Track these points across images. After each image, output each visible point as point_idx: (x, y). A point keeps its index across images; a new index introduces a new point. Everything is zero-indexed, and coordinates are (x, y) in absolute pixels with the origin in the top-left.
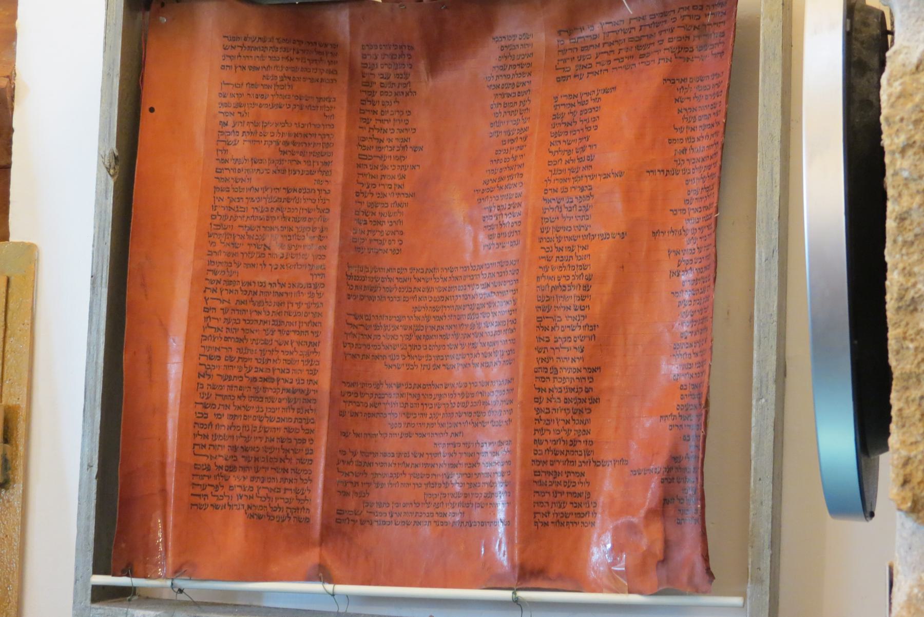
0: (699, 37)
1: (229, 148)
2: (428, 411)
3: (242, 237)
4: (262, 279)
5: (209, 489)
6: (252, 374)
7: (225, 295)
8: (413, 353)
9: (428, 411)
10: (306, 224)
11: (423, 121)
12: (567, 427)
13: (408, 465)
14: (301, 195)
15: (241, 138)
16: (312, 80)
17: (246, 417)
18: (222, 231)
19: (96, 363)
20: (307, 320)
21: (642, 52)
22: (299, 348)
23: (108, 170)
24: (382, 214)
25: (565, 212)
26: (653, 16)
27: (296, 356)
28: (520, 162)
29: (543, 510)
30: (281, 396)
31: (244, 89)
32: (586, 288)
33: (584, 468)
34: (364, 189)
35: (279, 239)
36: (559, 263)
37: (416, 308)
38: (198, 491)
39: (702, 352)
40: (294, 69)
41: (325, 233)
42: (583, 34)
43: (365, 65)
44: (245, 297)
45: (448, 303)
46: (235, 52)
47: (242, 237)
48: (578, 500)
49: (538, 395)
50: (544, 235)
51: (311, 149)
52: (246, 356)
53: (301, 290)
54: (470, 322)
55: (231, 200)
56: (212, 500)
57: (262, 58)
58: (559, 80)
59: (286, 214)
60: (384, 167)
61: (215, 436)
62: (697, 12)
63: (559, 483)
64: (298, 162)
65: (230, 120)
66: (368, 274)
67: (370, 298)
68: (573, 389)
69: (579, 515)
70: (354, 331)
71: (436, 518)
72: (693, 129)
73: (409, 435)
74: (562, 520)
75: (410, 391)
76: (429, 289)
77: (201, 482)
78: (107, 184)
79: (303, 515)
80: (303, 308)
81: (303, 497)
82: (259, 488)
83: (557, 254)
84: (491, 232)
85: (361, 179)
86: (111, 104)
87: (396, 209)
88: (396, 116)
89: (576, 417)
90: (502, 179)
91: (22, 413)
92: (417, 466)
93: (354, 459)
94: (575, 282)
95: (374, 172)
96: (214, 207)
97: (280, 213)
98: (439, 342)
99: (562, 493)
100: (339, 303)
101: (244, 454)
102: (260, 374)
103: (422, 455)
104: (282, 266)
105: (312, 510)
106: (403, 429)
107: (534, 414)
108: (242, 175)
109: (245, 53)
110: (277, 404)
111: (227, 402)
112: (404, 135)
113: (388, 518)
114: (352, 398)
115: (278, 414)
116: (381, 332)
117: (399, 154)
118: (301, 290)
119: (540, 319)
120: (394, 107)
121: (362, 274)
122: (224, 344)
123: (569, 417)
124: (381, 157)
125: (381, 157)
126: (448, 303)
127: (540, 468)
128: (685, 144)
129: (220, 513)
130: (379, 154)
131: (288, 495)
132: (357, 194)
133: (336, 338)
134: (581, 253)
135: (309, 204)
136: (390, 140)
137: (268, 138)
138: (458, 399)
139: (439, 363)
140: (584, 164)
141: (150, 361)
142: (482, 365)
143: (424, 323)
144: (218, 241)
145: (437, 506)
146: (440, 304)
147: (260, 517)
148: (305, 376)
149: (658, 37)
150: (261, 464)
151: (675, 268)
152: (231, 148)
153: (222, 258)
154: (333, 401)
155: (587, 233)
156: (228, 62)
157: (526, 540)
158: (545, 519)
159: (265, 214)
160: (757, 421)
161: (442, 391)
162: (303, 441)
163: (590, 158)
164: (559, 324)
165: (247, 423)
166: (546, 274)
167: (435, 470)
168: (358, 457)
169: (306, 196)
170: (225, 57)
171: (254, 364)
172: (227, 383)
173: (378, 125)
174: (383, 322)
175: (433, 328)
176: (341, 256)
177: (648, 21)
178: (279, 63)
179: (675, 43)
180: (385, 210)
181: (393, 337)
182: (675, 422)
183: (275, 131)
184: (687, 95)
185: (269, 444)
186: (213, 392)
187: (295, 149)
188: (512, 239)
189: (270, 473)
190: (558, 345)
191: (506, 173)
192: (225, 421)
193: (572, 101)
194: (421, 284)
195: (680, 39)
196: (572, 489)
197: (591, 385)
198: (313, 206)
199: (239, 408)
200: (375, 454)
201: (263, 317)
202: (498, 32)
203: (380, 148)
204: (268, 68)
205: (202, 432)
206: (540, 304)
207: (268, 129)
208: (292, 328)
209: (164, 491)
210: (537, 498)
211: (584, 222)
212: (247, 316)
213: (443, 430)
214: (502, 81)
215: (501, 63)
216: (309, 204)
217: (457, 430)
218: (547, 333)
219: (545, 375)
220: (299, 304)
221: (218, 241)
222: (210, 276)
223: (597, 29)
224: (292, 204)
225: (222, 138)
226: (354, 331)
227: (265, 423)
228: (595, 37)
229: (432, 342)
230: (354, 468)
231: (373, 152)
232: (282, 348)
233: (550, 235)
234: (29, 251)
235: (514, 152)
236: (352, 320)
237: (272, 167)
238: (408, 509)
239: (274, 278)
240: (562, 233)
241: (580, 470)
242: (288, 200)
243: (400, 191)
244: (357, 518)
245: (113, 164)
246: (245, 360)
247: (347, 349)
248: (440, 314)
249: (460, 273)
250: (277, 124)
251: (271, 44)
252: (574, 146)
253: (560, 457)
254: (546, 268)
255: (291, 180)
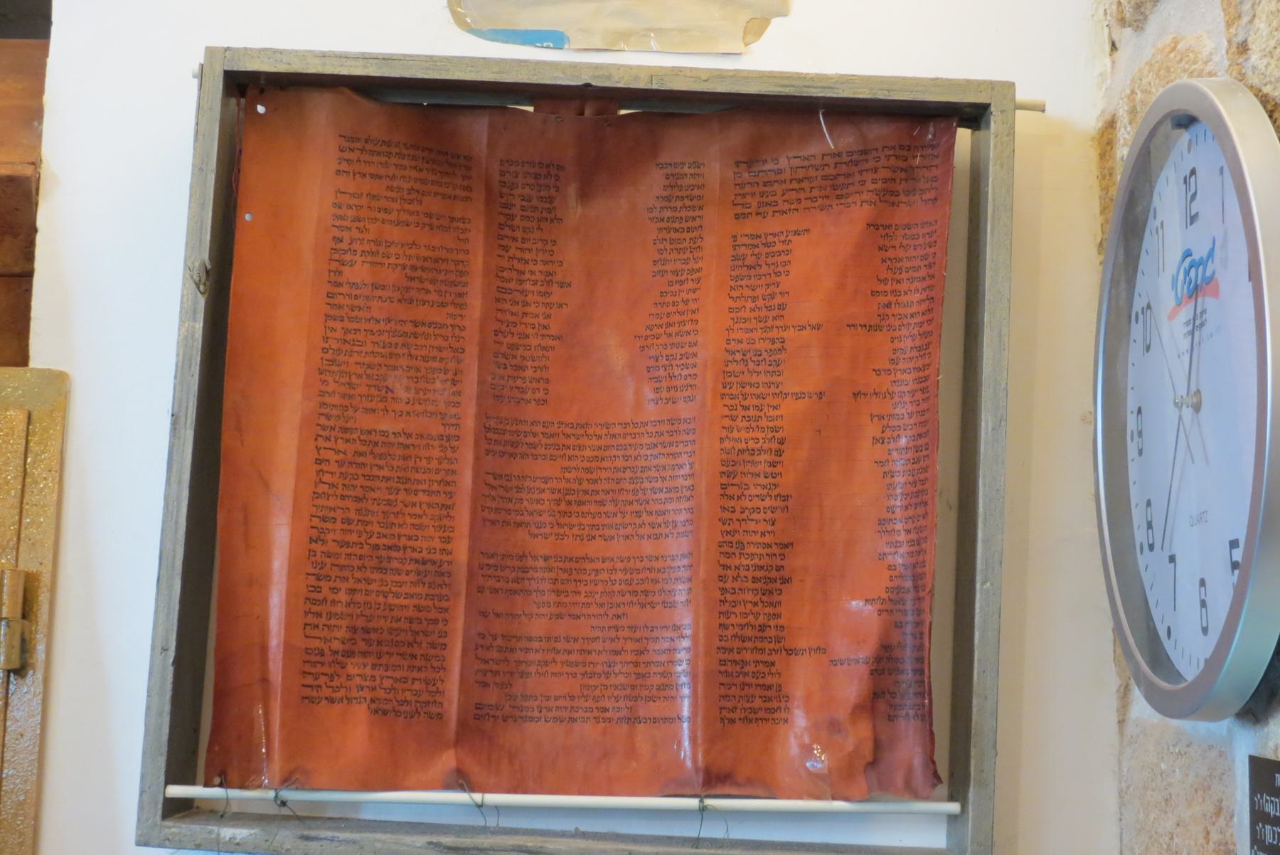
0: (906, 180)
1: (343, 268)
2: (582, 589)
3: (360, 376)
4: (384, 427)
5: (323, 680)
6: (374, 541)
7: (341, 445)
8: (562, 521)
9: (582, 589)
10: (436, 364)
11: (571, 254)
12: (756, 609)
13: (558, 652)
14: (431, 331)
15: (359, 259)
16: (444, 196)
17: (367, 593)
18: (335, 368)
19: (176, 522)
20: (438, 478)
21: (838, 192)
22: (431, 511)
23: (198, 285)
24: (524, 358)
25: (751, 365)
26: (850, 153)
27: (425, 521)
28: (693, 306)
29: (729, 705)
30: (409, 568)
31: (364, 201)
32: (779, 453)
33: (774, 657)
34: (504, 328)
35: (405, 381)
36: (746, 424)
37: (565, 469)
38: (309, 680)
39: (919, 530)
40: (423, 182)
41: (458, 377)
42: (767, 167)
43: (503, 184)
44: (364, 448)
45: (605, 464)
46: (353, 156)
47: (360, 376)
48: (768, 693)
49: (722, 572)
50: (727, 391)
51: (441, 277)
52: (366, 518)
53: (431, 442)
54: (632, 487)
55: (347, 331)
56: (326, 692)
57: (386, 165)
58: (737, 217)
59: (413, 352)
60: (526, 304)
61: (331, 615)
62: (905, 153)
63: (746, 674)
64: (428, 292)
65: (346, 235)
66: (508, 428)
67: (511, 455)
68: (762, 567)
69: (768, 710)
70: (493, 493)
71: (596, 714)
72: (898, 282)
73: (560, 616)
74: (751, 716)
75: (561, 565)
76: (580, 448)
77: (313, 670)
78: (195, 303)
79: (434, 709)
80: (434, 464)
81: (434, 689)
82: (382, 678)
83: (743, 413)
84: (658, 385)
85: (499, 315)
86: (203, 206)
87: (540, 353)
88: (540, 245)
89: (765, 598)
90: (669, 325)
91: (46, 579)
92: (570, 652)
93: (495, 644)
94: (766, 446)
95: (515, 309)
96: (326, 339)
97: (405, 351)
98: (593, 508)
99: (750, 685)
100: (477, 459)
101: (366, 636)
102: (384, 541)
103: (576, 640)
104: (408, 413)
105: (446, 705)
106: (553, 610)
107: (718, 595)
108: (360, 302)
109: (366, 157)
110: (403, 578)
111: (347, 573)
112: (549, 268)
113: (536, 714)
114: (491, 572)
115: (405, 589)
116: (524, 495)
117: (543, 289)
118: (431, 442)
119: (724, 487)
120: (537, 234)
121: (501, 426)
122: (340, 503)
123: (757, 599)
124: (522, 292)
125: (522, 292)
126: (605, 464)
127: (726, 656)
128: (890, 298)
129: (337, 708)
130: (520, 288)
131: (417, 686)
132: (496, 333)
133: (474, 500)
134: (772, 413)
135: (440, 342)
136: (532, 273)
137: (393, 260)
138: (620, 576)
139: (594, 532)
140: (775, 313)
141: (246, 521)
142: (649, 537)
143: (576, 486)
144: (330, 380)
145: (596, 699)
146: (594, 464)
147: (385, 713)
148: (437, 544)
149: (857, 177)
150: (385, 649)
151: (879, 435)
152: (346, 270)
153: (336, 400)
154: (471, 575)
155: (778, 391)
156: (344, 166)
157: (711, 740)
158: (732, 715)
159: (387, 350)
160: (981, 608)
161: (599, 565)
162: (435, 621)
163: (782, 307)
164: (746, 492)
165: (368, 598)
166: (731, 435)
167: (593, 657)
168: (499, 641)
169: (437, 332)
170: (341, 160)
171: (376, 528)
172: (346, 550)
173: (519, 254)
174: (528, 483)
175: (586, 492)
176: (479, 405)
177: (845, 158)
178: (406, 173)
179: (879, 185)
180: (527, 353)
181: (538, 501)
182: (885, 607)
183: (401, 252)
184: (893, 243)
185: (394, 625)
186: (328, 561)
187: (424, 275)
188: (686, 394)
189: (395, 660)
190: (744, 516)
191: (677, 318)
192: (343, 597)
193: (755, 242)
194: (572, 441)
195: (885, 181)
196: (761, 681)
197: (782, 563)
198: (444, 344)
199: (359, 581)
200: (519, 639)
201: (385, 473)
202: (664, 158)
203: (521, 282)
204: (393, 177)
205: (314, 608)
206: (725, 469)
207: (392, 250)
208: (421, 487)
209: (265, 680)
210: (723, 691)
211: (775, 379)
212: (367, 471)
213: (602, 611)
214: (668, 214)
215: (665, 194)
216: (440, 342)
217: (620, 611)
218: (732, 503)
219: (730, 550)
220: (429, 459)
221: (330, 380)
222: (323, 421)
223: (783, 163)
224: (420, 341)
225: (336, 256)
226: (493, 493)
227: (391, 600)
228: (780, 172)
229: (585, 508)
230: (494, 654)
231: (512, 285)
232: (409, 510)
233: (733, 391)
234: (58, 382)
235: (684, 295)
236: (490, 479)
237: (397, 295)
238: (561, 703)
239: (399, 427)
240: (748, 389)
241: (770, 659)
242: (415, 335)
243: (545, 332)
244: (498, 713)
245: (204, 278)
246: (366, 523)
247: (486, 514)
248: (594, 476)
249: (618, 430)
250: (403, 245)
251: (397, 150)
252: (759, 292)
253: (749, 645)
254: (731, 429)
255: (420, 313)
